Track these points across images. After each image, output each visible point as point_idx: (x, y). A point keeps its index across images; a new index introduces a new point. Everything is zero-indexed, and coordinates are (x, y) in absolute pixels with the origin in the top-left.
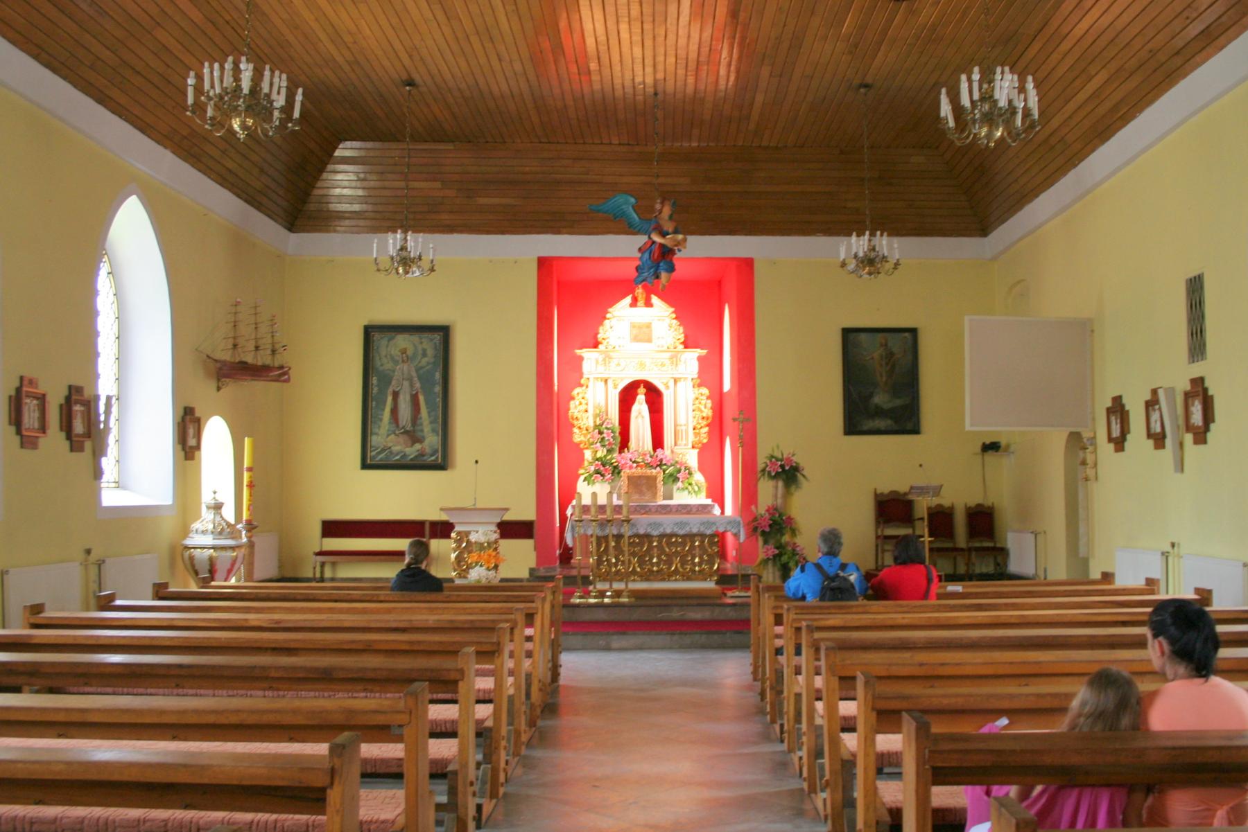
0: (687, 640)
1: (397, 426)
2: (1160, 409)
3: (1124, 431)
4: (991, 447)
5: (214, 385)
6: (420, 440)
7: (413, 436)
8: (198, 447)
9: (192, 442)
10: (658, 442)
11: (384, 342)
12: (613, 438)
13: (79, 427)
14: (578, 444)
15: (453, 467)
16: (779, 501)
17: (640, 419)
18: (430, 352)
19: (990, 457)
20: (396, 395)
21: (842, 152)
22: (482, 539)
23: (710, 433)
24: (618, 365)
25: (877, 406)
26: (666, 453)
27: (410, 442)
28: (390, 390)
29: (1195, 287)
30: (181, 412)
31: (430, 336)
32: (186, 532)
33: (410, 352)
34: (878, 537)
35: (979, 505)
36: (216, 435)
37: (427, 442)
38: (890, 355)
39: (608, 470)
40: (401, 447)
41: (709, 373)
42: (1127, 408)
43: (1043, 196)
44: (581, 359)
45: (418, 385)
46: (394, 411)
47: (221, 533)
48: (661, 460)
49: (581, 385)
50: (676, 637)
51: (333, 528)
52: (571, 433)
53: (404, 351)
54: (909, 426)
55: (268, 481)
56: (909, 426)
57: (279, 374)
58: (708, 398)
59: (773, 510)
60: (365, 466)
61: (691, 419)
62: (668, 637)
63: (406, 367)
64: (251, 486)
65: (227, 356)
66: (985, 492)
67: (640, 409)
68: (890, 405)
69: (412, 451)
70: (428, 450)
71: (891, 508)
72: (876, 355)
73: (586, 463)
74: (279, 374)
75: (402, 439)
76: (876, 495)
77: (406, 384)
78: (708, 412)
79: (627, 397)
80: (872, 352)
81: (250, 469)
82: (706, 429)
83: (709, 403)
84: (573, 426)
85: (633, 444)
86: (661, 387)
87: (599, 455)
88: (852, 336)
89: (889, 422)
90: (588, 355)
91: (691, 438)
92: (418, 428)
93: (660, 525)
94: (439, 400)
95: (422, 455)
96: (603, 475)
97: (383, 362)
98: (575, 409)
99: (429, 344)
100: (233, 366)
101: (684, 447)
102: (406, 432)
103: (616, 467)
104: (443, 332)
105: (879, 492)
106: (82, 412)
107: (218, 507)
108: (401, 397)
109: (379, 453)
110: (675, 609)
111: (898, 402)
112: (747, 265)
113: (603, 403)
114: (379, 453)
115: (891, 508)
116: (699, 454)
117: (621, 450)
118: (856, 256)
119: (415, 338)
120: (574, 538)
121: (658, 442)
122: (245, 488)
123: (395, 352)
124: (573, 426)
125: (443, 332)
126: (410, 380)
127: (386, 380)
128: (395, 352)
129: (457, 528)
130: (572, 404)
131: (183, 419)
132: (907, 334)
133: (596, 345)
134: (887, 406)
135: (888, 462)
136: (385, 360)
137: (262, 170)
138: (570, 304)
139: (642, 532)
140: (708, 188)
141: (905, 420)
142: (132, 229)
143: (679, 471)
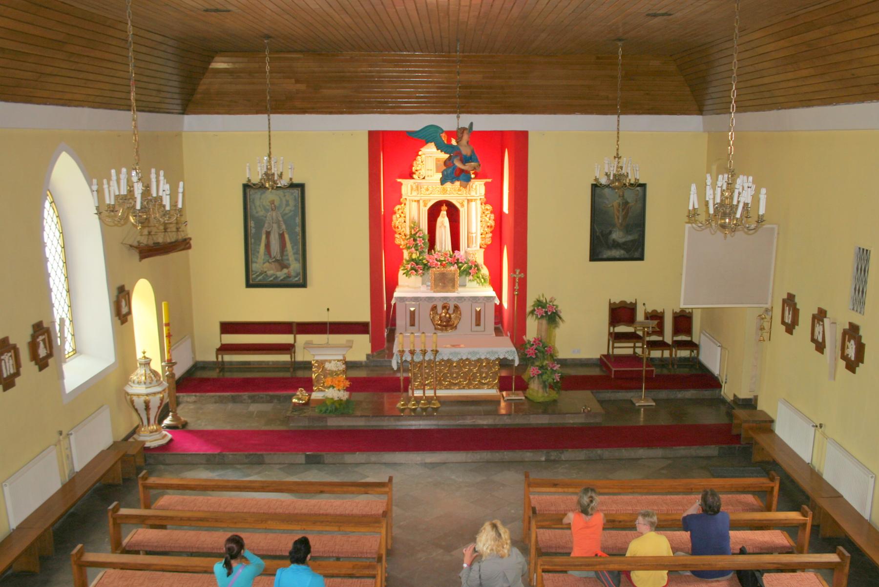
2: (823, 325)
3: (795, 322)
8: (129, 313)
9: (124, 310)
10: (456, 246)
12: (423, 243)
13: (42, 352)
14: (399, 245)
16: (543, 334)
17: (443, 229)
18: (292, 203)
20: (268, 234)
22: (335, 369)
23: (492, 238)
24: (427, 190)
25: (614, 241)
26: (461, 254)
28: (264, 231)
29: (863, 255)
30: (115, 293)
32: (126, 380)
33: (277, 203)
34: (610, 334)
37: (292, 267)
38: (626, 203)
39: (420, 267)
40: (272, 271)
41: (493, 197)
42: (798, 307)
44: (401, 184)
45: (284, 227)
46: (268, 246)
48: (458, 260)
49: (401, 204)
51: (227, 328)
52: (394, 238)
53: (272, 202)
54: (637, 255)
57: (184, 244)
58: (491, 213)
59: (538, 341)
61: (479, 227)
63: (274, 214)
64: (169, 336)
65: (144, 241)
67: (443, 221)
68: (624, 240)
69: (282, 274)
70: (293, 274)
71: (621, 313)
72: (615, 204)
73: (404, 262)
75: (273, 266)
76: (610, 304)
77: (275, 226)
78: (492, 223)
79: (434, 212)
80: (612, 201)
81: (167, 325)
82: (490, 235)
83: (492, 216)
84: (395, 233)
85: (438, 247)
86: (458, 206)
87: (414, 256)
89: (622, 252)
90: (407, 186)
91: (479, 241)
92: (285, 258)
93: (459, 353)
94: (300, 237)
95: (289, 276)
96: (416, 271)
97: (258, 211)
98: (397, 220)
100: (151, 242)
101: (474, 249)
102: (277, 261)
103: (425, 265)
105: (612, 302)
106: (44, 340)
109: (258, 276)
110: (469, 417)
112: (522, 137)
113: (416, 218)
114: (258, 276)
115: (621, 313)
116: (485, 252)
121: (456, 246)
123: (267, 203)
124: (395, 233)
126: (278, 223)
127: (260, 223)
128: (267, 203)
130: (394, 217)
131: (118, 297)
132: (638, 188)
133: (410, 176)
135: (620, 280)
136: (259, 209)
137: (159, 91)
138: (390, 156)
139: (445, 358)
141: (634, 250)
142: (66, 172)
143: (470, 268)
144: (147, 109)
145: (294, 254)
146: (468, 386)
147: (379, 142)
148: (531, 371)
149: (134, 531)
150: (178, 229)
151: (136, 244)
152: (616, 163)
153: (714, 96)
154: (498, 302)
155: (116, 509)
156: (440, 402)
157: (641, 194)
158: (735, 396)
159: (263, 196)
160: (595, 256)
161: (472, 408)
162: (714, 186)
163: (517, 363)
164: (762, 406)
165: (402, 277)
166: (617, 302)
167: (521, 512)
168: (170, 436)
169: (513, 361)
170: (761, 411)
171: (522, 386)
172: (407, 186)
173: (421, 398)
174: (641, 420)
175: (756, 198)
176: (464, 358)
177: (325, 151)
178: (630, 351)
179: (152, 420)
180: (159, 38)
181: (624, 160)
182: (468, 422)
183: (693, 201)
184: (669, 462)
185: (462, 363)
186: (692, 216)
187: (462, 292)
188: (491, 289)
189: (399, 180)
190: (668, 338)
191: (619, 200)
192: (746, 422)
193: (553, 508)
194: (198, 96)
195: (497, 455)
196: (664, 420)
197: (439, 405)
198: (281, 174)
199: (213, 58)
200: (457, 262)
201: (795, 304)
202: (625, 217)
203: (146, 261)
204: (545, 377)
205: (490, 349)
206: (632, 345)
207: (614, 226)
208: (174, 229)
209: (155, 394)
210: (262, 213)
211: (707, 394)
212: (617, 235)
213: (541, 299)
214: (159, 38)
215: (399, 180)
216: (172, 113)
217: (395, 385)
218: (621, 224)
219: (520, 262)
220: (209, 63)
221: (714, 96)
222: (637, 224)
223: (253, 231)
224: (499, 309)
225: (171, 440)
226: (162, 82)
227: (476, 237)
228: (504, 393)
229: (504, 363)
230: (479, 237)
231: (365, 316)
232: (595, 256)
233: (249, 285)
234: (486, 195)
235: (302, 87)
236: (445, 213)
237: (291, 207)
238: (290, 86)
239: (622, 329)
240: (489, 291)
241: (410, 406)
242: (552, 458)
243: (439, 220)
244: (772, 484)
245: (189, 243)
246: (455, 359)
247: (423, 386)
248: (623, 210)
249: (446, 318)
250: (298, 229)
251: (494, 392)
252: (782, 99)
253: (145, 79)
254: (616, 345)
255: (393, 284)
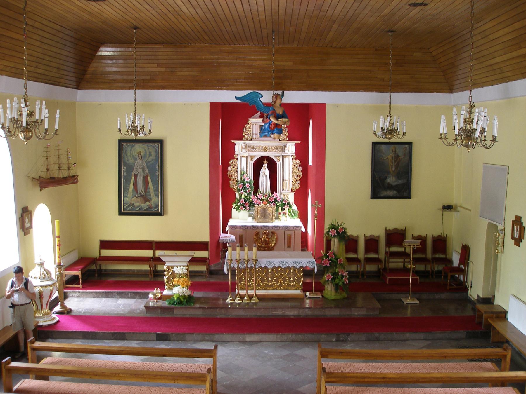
0: (285, 337)
1: (137, 192)
4: (448, 208)
5: (38, 188)
6: (149, 200)
7: (145, 198)
8: (31, 227)
9: (27, 225)
10: (274, 189)
11: (129, 148)
15: (167, 214)
18: (153, 154)
19: (447, 213)
20: (136, 176)
21: (376, 50)
22: (181, 272)
25: (389, 184)
26: (278, 195)
27: (144, 201)
28: (133, 174)
30: (21, 211)
31: (153, 145)
35: (439, 236)
36: (42, 215)
37: (153, 201)
38: (397, 156)
40: (138, 203)
41: (301, 154)
43: (485, 88)
44: (234, 144)
45: (147, 171)
46: (135, 185)
47: (44, 278)
49: (234, 158)
50: (279, 336)
51: (105, 244)
53: (139, 153)
54: (405, 194)
55: (69, 233)
56: (405, 194)
60: (121, 213)
62: (275, 336)
64: (59, 245)
65: (44, 175)
66: (443, 227)
67: (265, 171)
68: (395, 184)
69: (145, 206)
70: (153, 205)
74: (72, 179)
75: (139, 199)
77: (141, 170)
79: (258, 165)
80: (388, 155)
81: (58, 237)
83: (301, 168)
85: (261, 190)
86: (276, 160)
88: (377, 146)
89: (395, 192)
93: (273, 262)
94: (158, 179)
95: (150, 207)
96: (245, 207)
99: (153, 149)
102: (141, 196)
103: (251, 203)
104: (160, 142)
105: (387, 229)
107: (42, 264)
108: (139, 177)
109: (127, 207)
110: (280, 310)
111: (400, 182)
114: (127, 207)
117: (255, 194)
118: (382, 129)
119: (145, 146)
120: (228, 270)
121: (274, 189)
122: (57, 247)
123: (135, 154)
125: (160, 142)
127: (130, 168)
128: (135, 154)
129: (167, 264)
132: (406, 146)
133: (241, 138)
134: (394, 184)
136: (130, 158)
137: (58, 69)
140: (303, 67)
141: (404, 191)
144: (50, 82)
145: (154, 191)
146: (280, 287)
147: (218, 111)
148: (327, 276)
149: (23, 380)
150: (69, 168)
151: (37, 177)
152: (388, 120)
153: (460, 77)
154: (303, 230)
155: (8, 362)
156: (258, 298)
157: (408, 150)
158: (478, 296)
159: (133, 149)
160: (375, 195)
161: (282, 304)
162: (459, 115)
163: (316, 271)
164: (498, 301)
165: (234, 212)
166: (391, 229)
167: (316, 376)
168: (57, 319)
169: (313, 270)
170: (497, 305)
171: (320, 288)
172: (239, 145)
173: (244, 296)
174: (409, 313)
175: (491, 125)
176: (277, 266)
177: (180, 119)
178: (401, 265)
179: (44, 306)
180: (58, 28)
181: (394, 118)
182: (279, 312)
183: (443, 128)
184: (429, 342)
185: (276, 269)
186: (443, 137)
187: (276, 223)
188: (299, 221)
189: (233, 141)
190: (429, 254)
191: (392, 154)
192: (485, 312)
193: (340, 371)
194: (88, 76)
195: (300, 337)
196: (426, 313)
197: (258, 301)
198: (143, 126)
199: (99, 48)
200: (275, 200)
201: (522, 224)
202: (397, 166)
203: (46, 190)
204: (337, 280)
205: (296, 260)
206: (402, 260)
207: (388, 173)
208: (67, 168)
209: (46, 286)
210: (131, 161)
211: (457, 295)
212: (391, 180)
213: (334, 223)
214: (58, 28)
215: (233, 141)
216: (69, 87)
217: (226, 288)
218: (394, 172)
219: (320, 198)
220: (97, 50)
221: (460, 77)
222: (405, 171)
223: (125, 173)
224: (305, 235)
225: (58, 322)
226: (61, 62)
227: (289, 183)
228: (308, 294)
229: (307, 272)
230: (291, 183)
231: (205, 237)
232: (375, 195)
233: (121, 213)
234: (296, 152)
235: (162, 69)
236: (266, 165)
237: (153, 157)
238: (153, 68)
239: (394, 249)
240: (297, 222)
241: (236, 301)
242: (341, 339)
243: (262, 170)
244: (505, 353)
245: (77, 179)
246: (270, 267)
247: (246, 287)
248: (395, 161)
249: (263, 239)
250: (158, 173)
251: (298, 292)
252: (509, 74)
253: (48, 58)
254: (391, 260)
255: (227, 216)
